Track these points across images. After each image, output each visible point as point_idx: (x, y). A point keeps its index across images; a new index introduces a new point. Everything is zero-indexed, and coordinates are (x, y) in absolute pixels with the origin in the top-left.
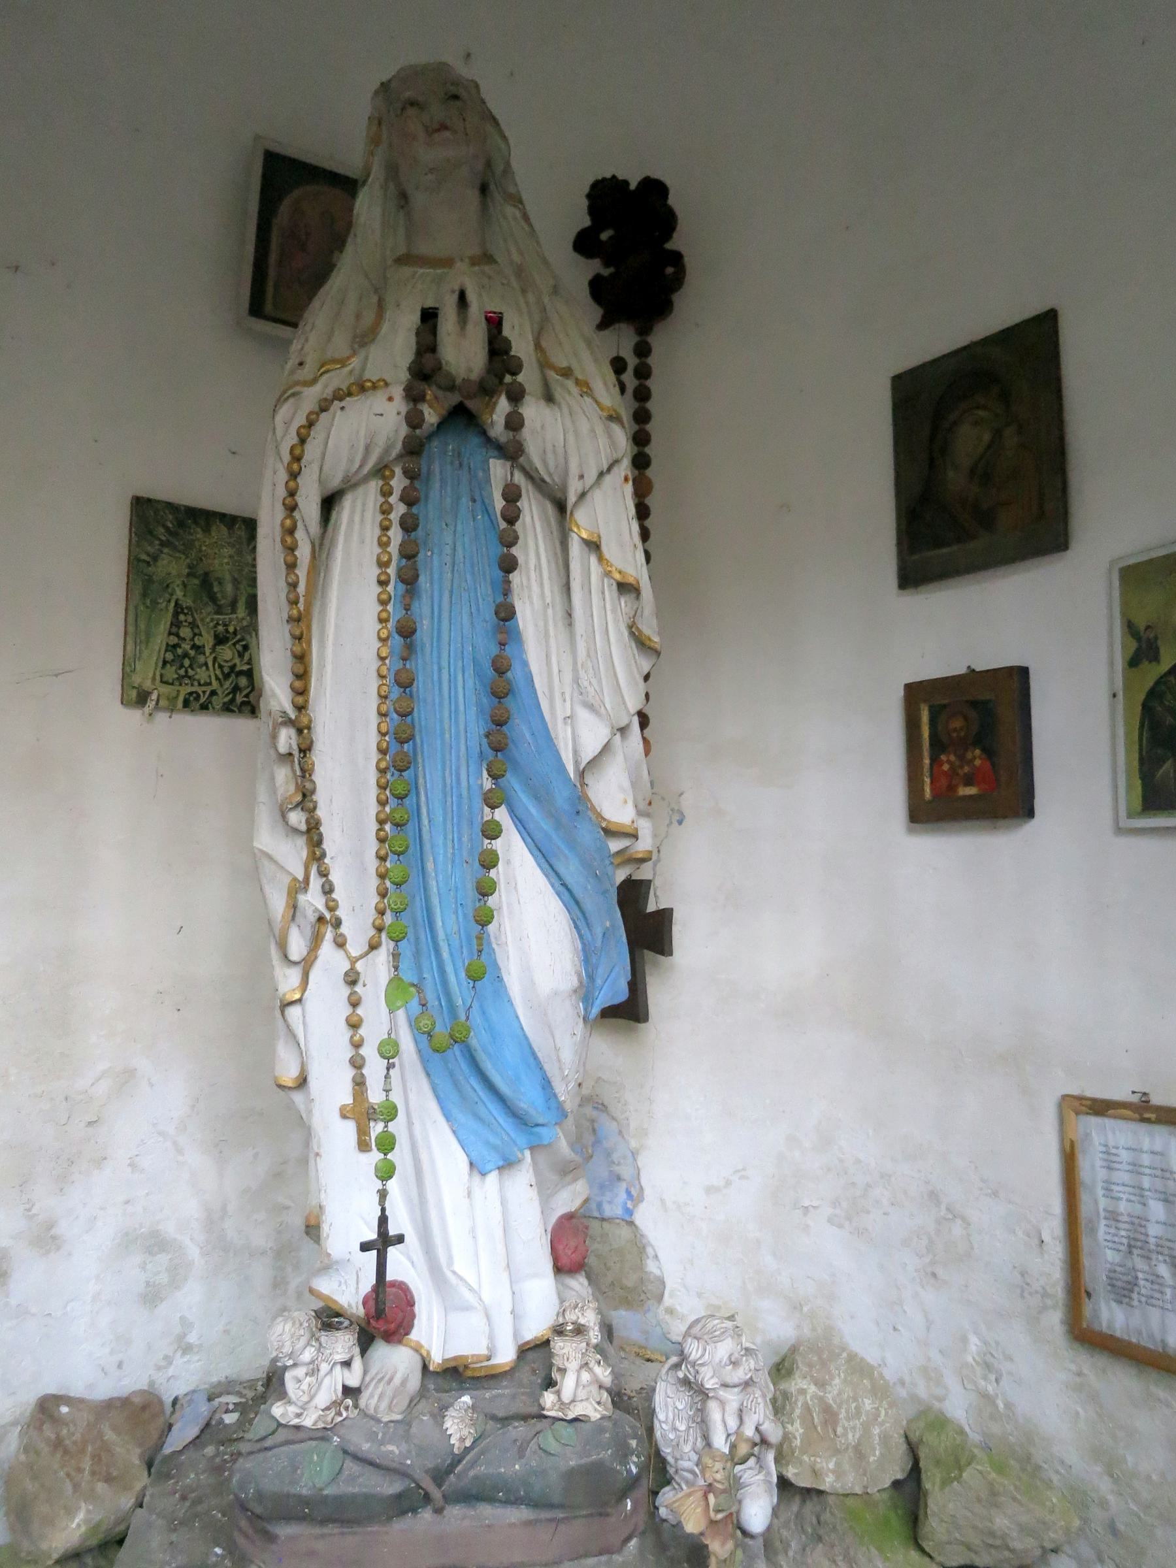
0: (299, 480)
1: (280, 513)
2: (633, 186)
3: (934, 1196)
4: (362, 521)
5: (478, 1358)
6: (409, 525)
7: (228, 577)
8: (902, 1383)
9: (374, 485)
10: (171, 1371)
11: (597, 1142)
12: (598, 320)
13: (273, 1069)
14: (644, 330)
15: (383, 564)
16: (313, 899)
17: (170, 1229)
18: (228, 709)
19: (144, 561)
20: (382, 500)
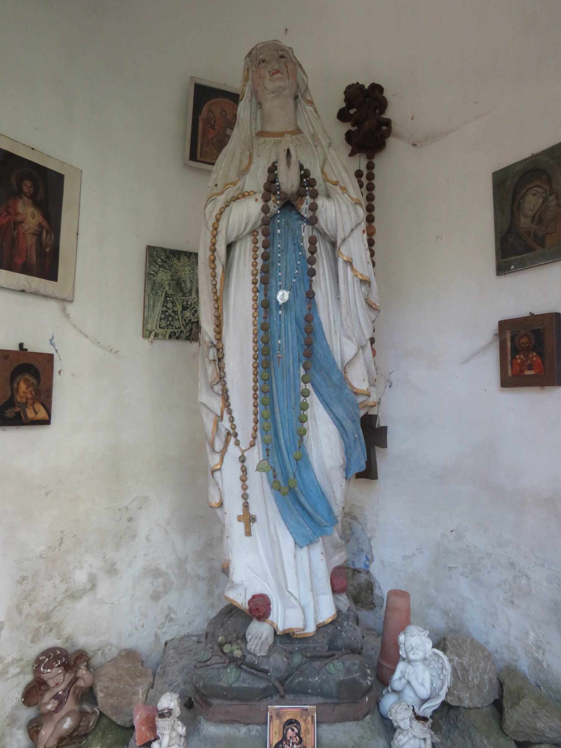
0: (216, 238)
1: (209, 253)
2: (366, 87)
3: (512, 565)
4: (245, 256)
5: (299, 630)
6: (265, 257)
7: (188, 280)
8: (497, 652)
9: (250, 239)
10: (164, 629)
11: (352, 533)
12: (349, 152)
13: (207, 498)
14: (370, 157)
15: (255, 275)
16: (226, 424)
17: (163, 567)
18: (188, 339)
19: (152, 274)
20: (254, 245)
